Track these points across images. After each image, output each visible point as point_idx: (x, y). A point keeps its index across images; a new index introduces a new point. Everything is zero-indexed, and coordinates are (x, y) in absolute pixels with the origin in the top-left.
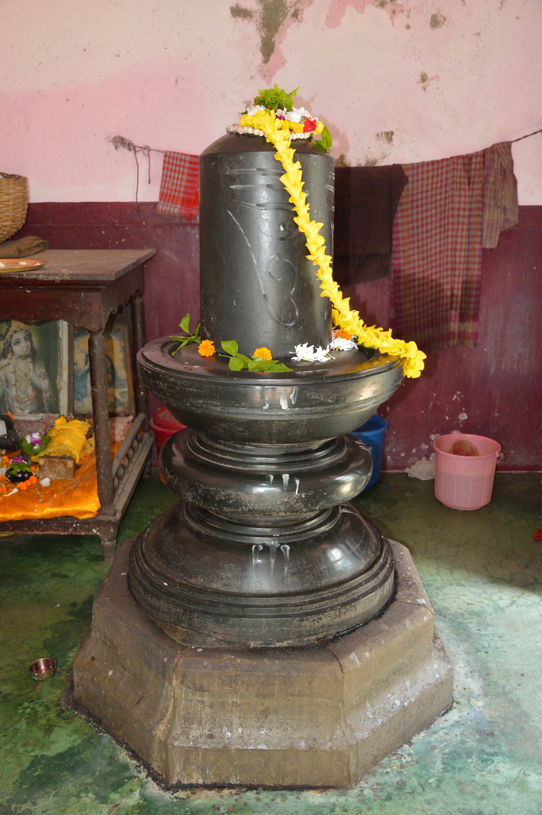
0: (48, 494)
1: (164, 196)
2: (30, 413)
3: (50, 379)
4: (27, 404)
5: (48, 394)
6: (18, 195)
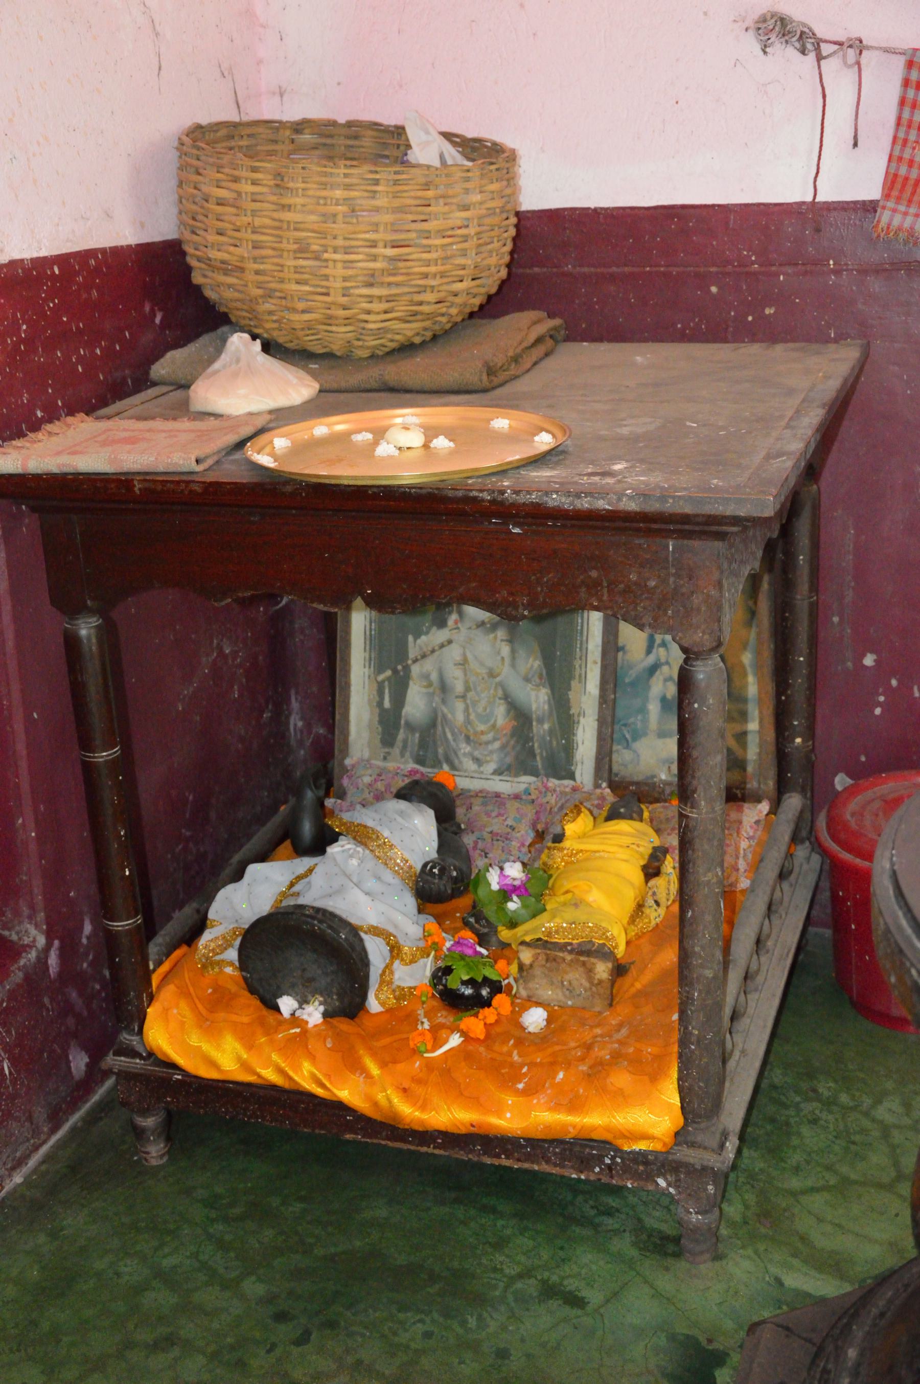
1: (898, 186)
3: (552, 689)
4: (490, 747)
5: (546, 726)
6: (491, 204)
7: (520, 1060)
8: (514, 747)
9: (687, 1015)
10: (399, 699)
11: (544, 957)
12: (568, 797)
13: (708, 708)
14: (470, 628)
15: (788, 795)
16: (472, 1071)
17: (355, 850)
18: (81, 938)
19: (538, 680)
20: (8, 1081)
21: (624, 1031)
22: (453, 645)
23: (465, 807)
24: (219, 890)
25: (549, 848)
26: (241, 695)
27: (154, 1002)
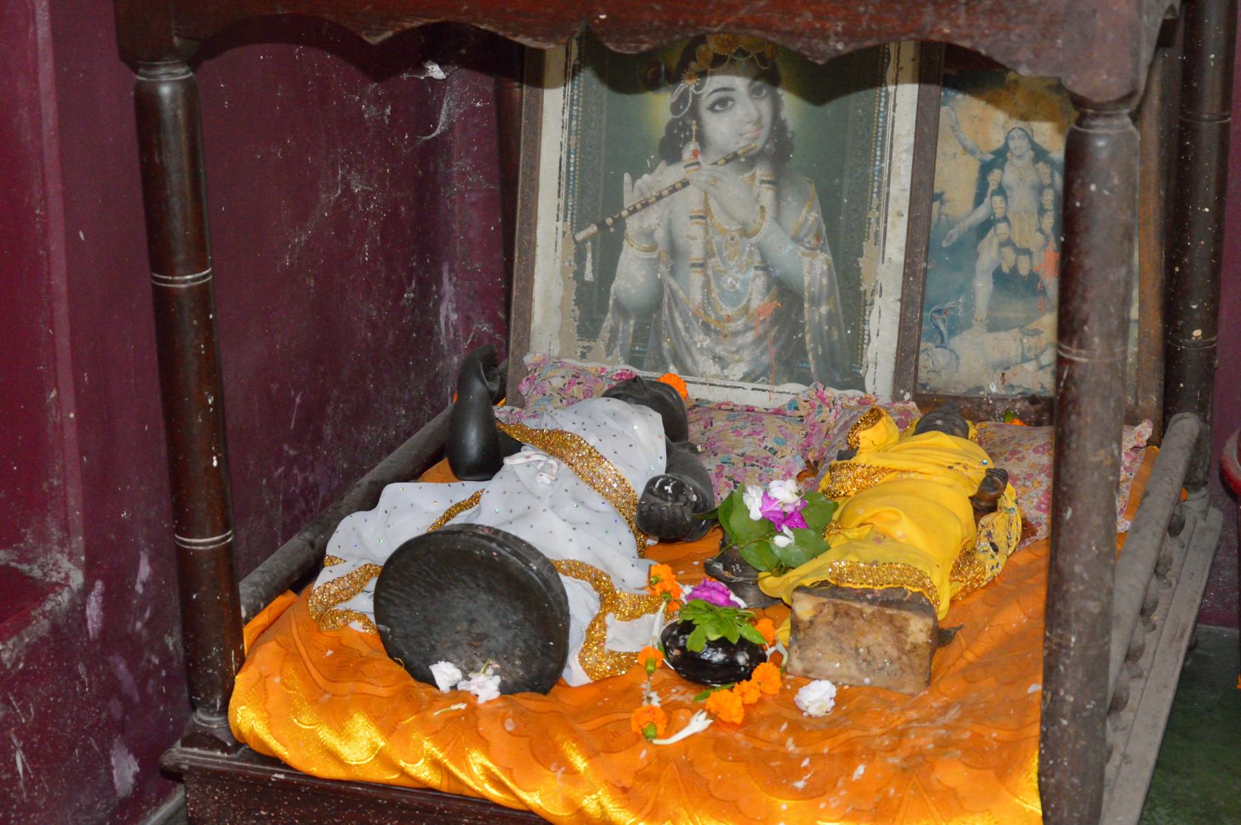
0: (830, 756)
2: (749, 377)
4: (740, 340)
5: (824, 310)
7: (798, 751)
8: (776, 339)
9: (1058, 673)
10: (607, 270)
11: (832, 609)
12: (855, 412)
13: (1111, 191)
14: (715, 163)
15: (1178, 415)
16: (725, 764)
17: (546, 463)
18: (133, 584)
19: (814, 242)
20: (21, 784)
21: (953, 713)
22: (690, 189)
23: (702, 423)
24: (340, 518)
25: (832, 469)
26: (373, 260)
27: (246, 665)
